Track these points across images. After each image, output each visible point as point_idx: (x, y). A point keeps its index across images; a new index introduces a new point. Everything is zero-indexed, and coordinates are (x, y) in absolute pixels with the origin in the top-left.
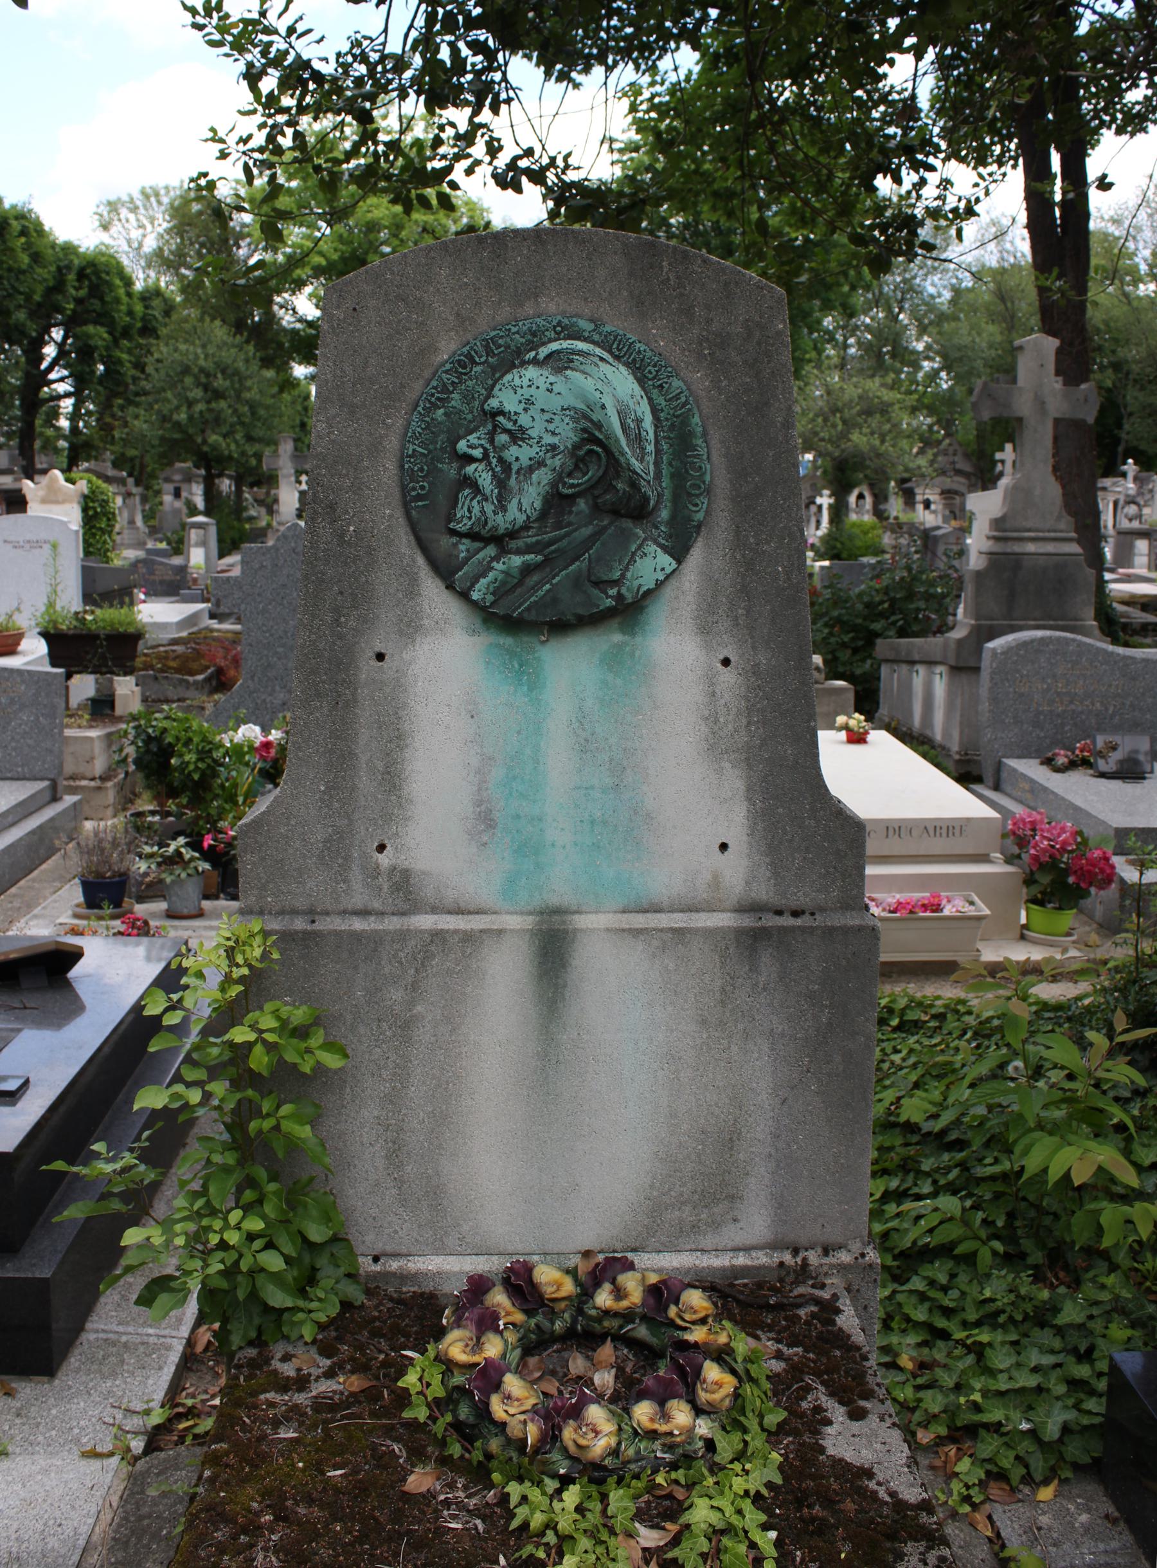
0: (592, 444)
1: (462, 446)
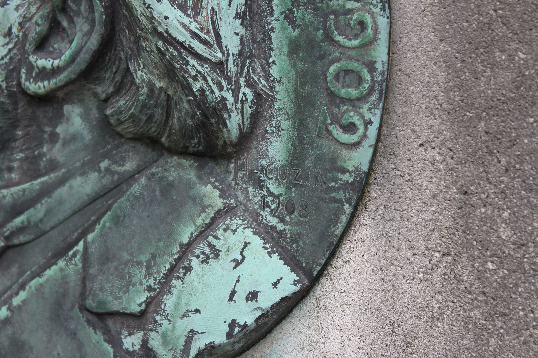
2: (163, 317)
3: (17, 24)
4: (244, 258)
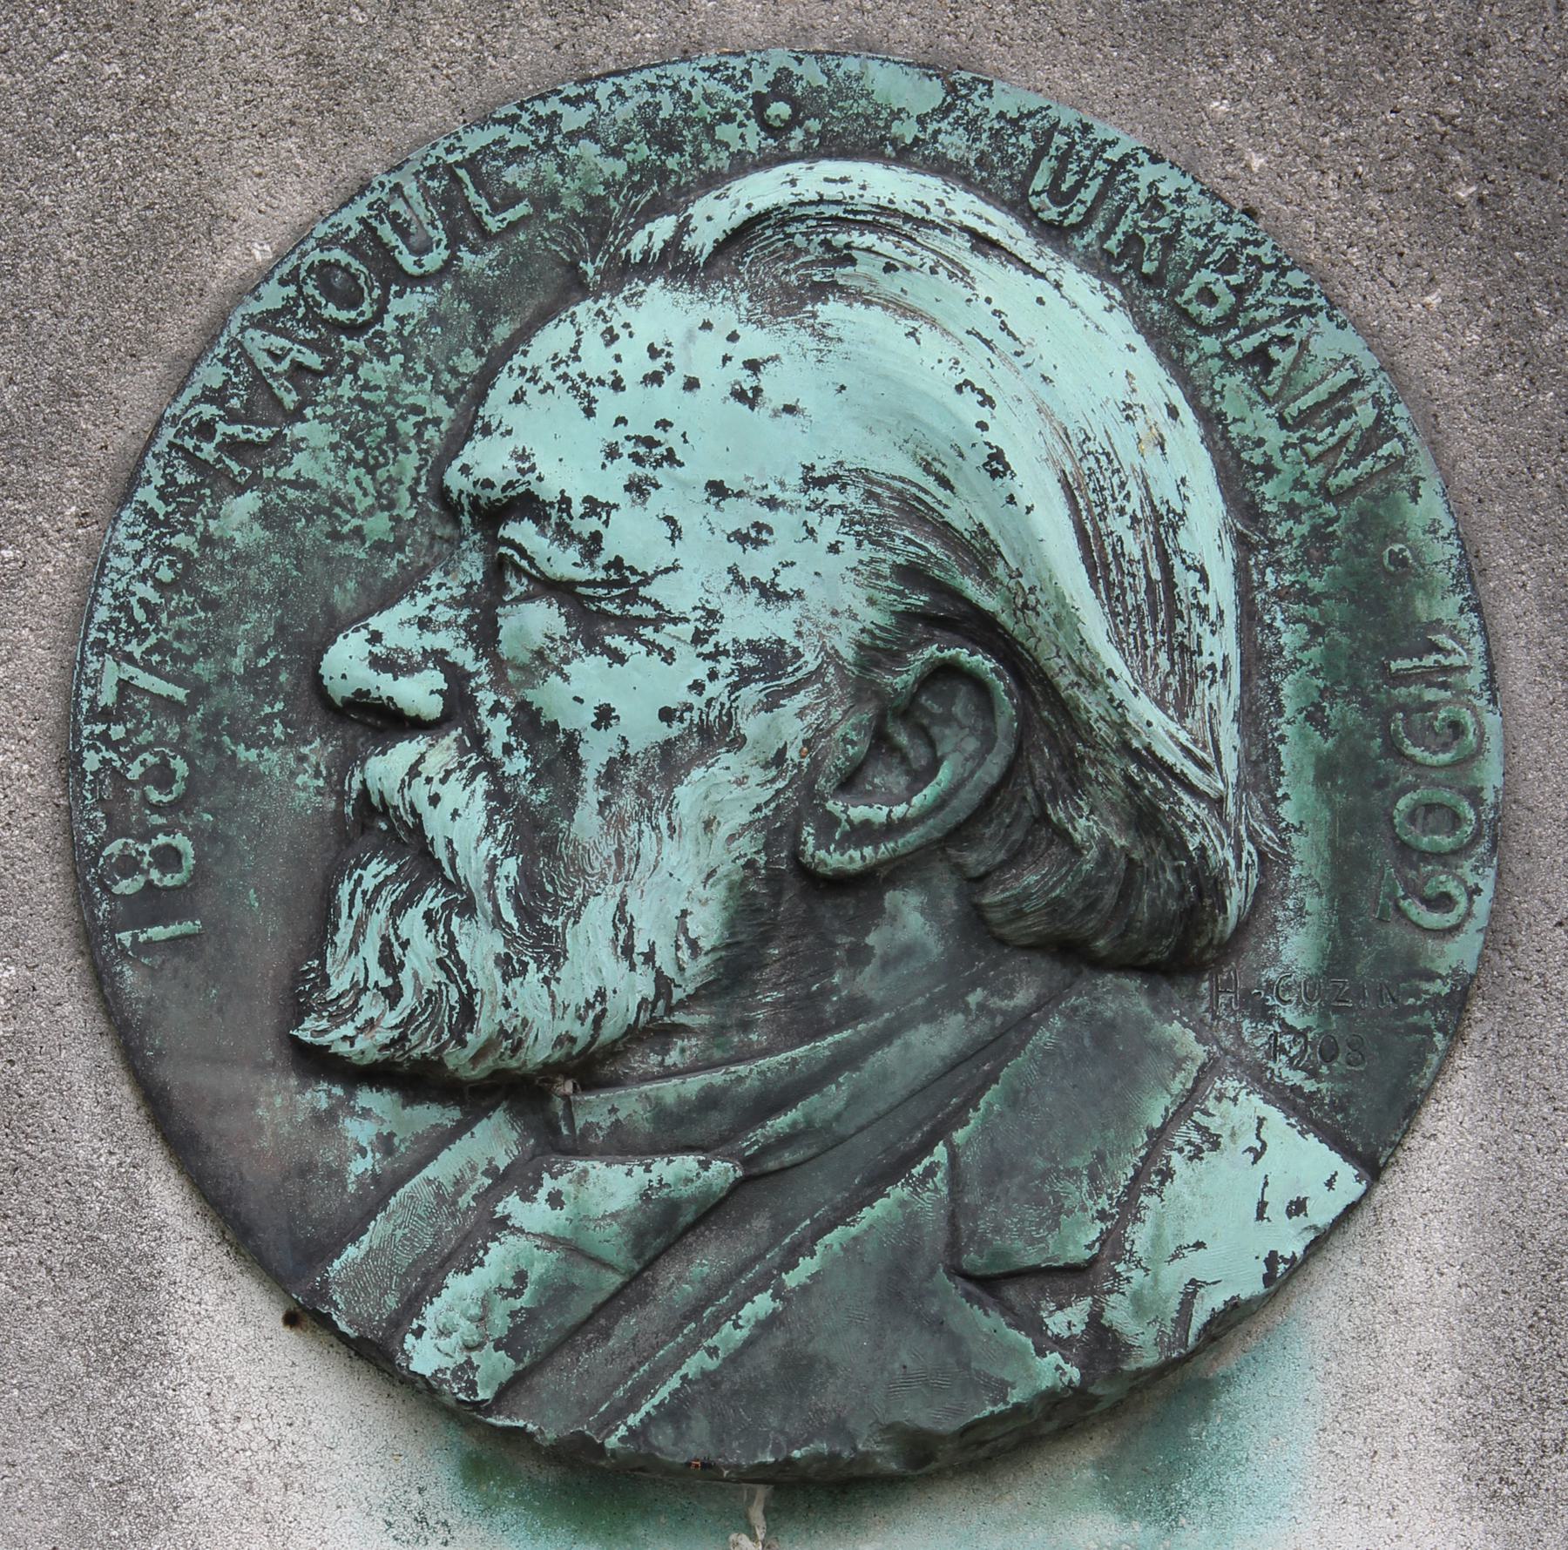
0: (953, 640)
1: (347, 663)
2: (1132, 1265)
3: (799, 743)
4: (1264, 1146)
